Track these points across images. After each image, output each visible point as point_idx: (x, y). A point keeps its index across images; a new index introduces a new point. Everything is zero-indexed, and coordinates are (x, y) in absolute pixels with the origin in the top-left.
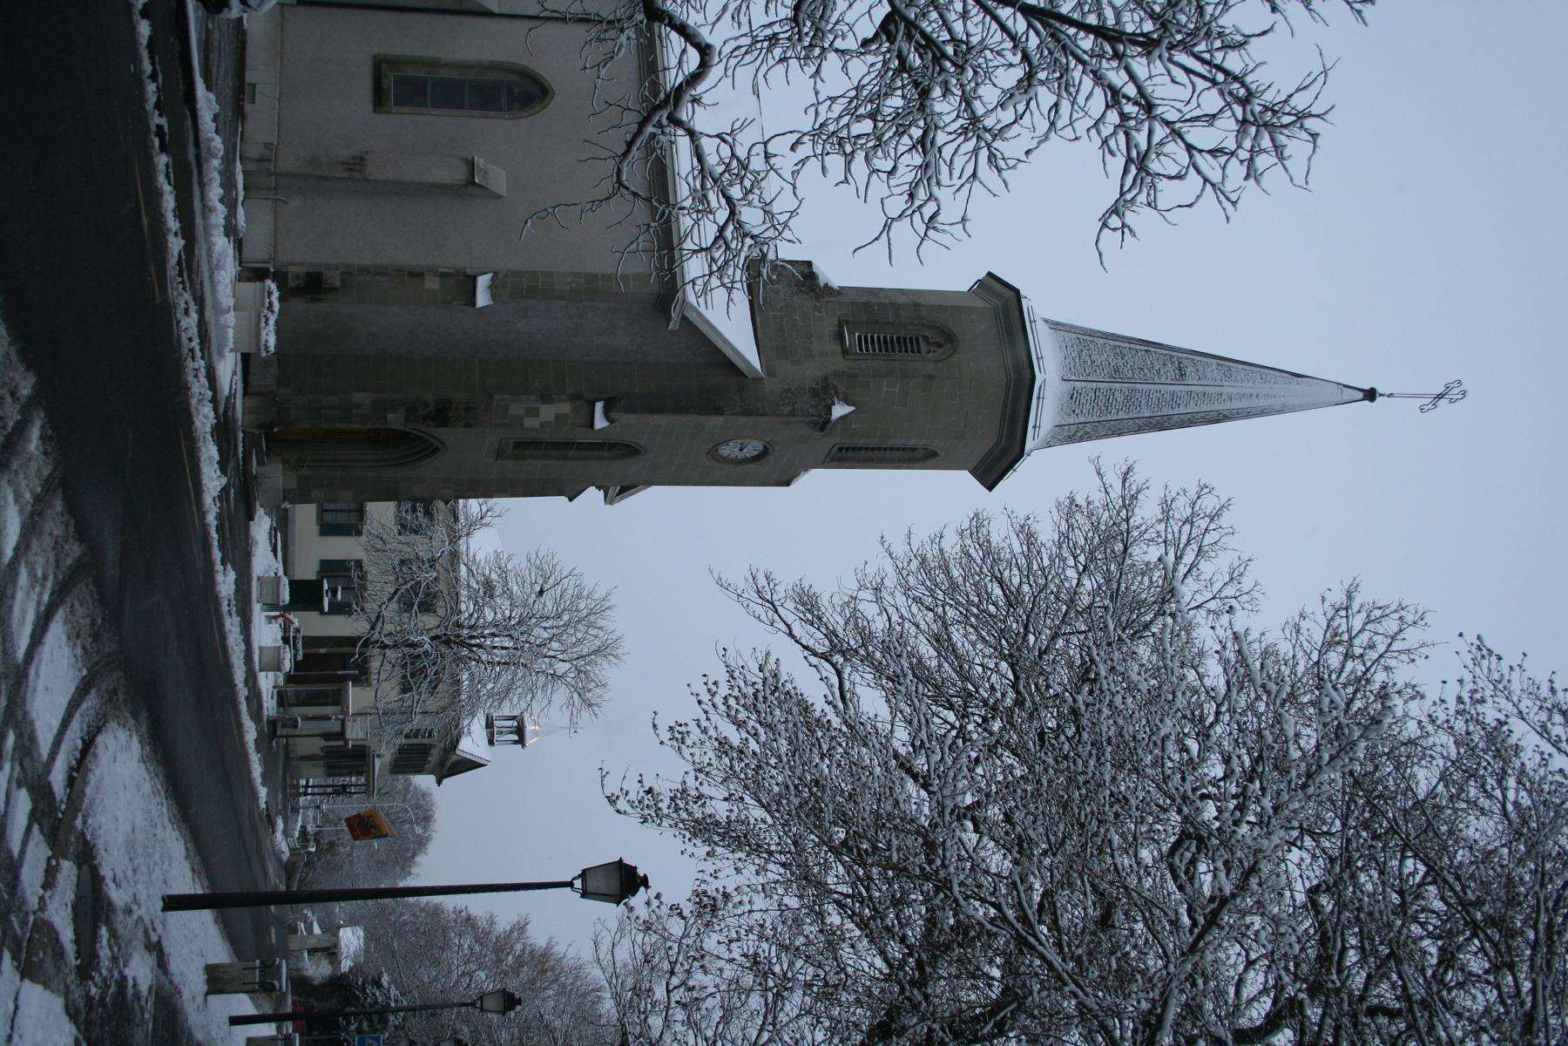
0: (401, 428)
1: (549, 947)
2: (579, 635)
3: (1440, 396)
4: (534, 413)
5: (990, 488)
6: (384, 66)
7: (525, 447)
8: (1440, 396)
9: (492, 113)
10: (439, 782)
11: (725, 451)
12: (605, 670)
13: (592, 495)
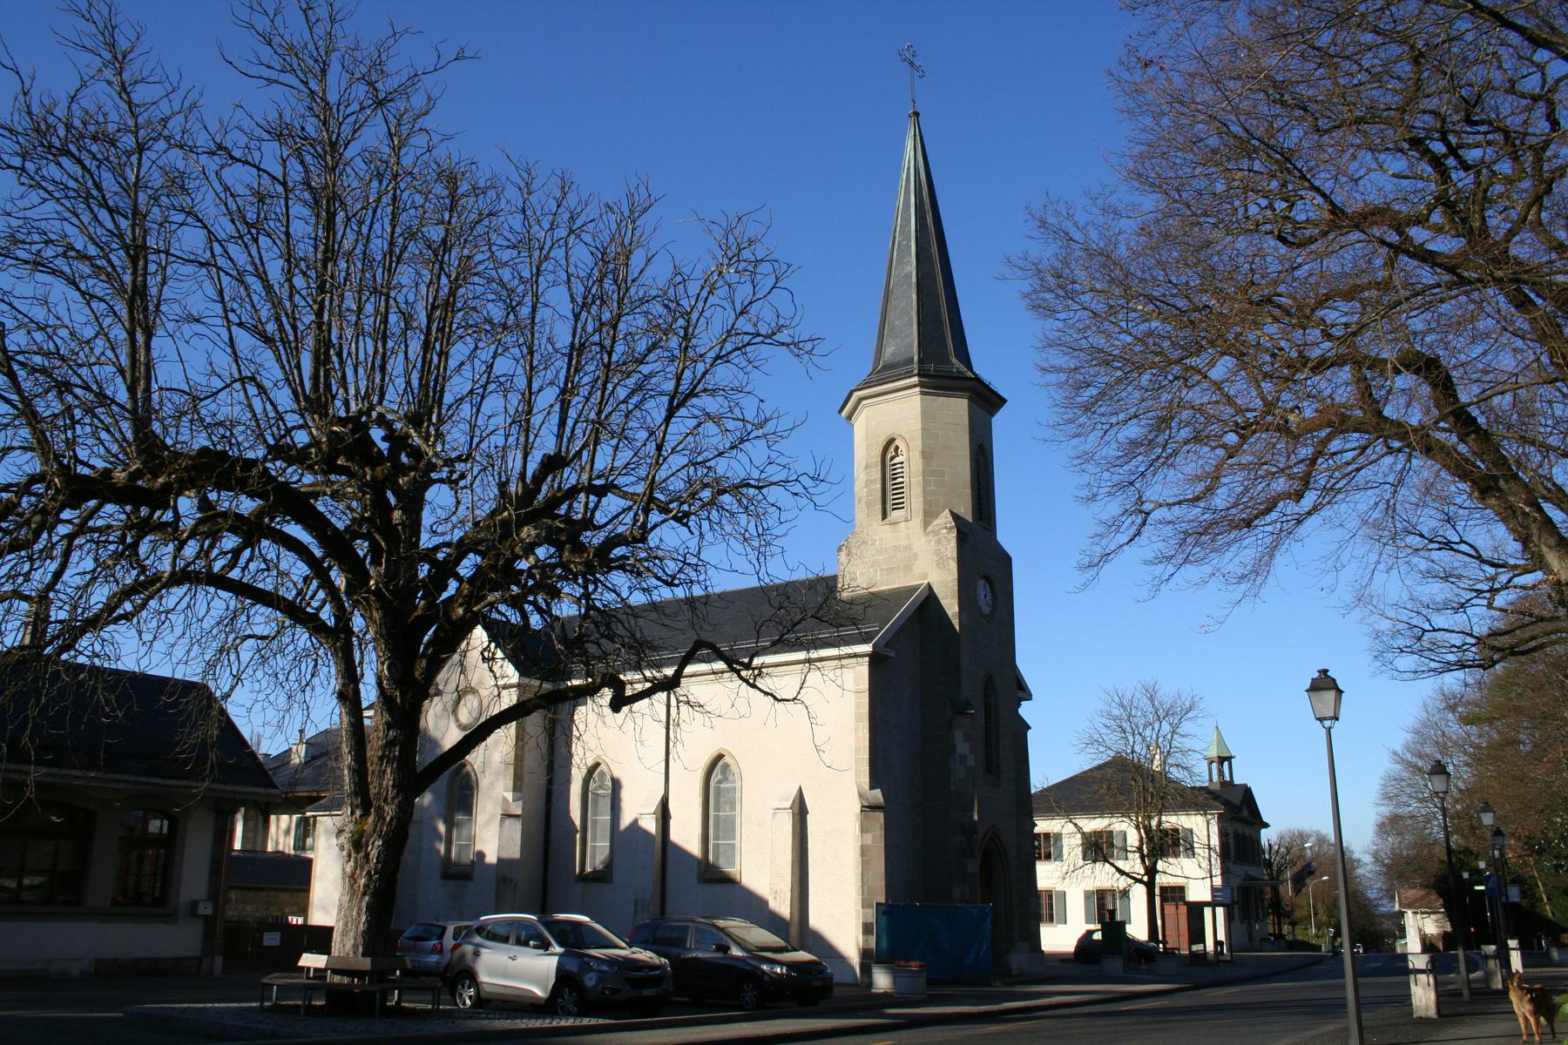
0: (979, 862)
1: (1416, 732)
2: (1139, 714)
3: (912, 64)
4: (963, 759)
5: (1004, 401)
6: (708, 876)
7: (990, 764)
8: (912, 64)
9: (738, 795)
10: (1266, 825)
11: (986, 610)
12: (1166, 694)
13: (1025, 710)
